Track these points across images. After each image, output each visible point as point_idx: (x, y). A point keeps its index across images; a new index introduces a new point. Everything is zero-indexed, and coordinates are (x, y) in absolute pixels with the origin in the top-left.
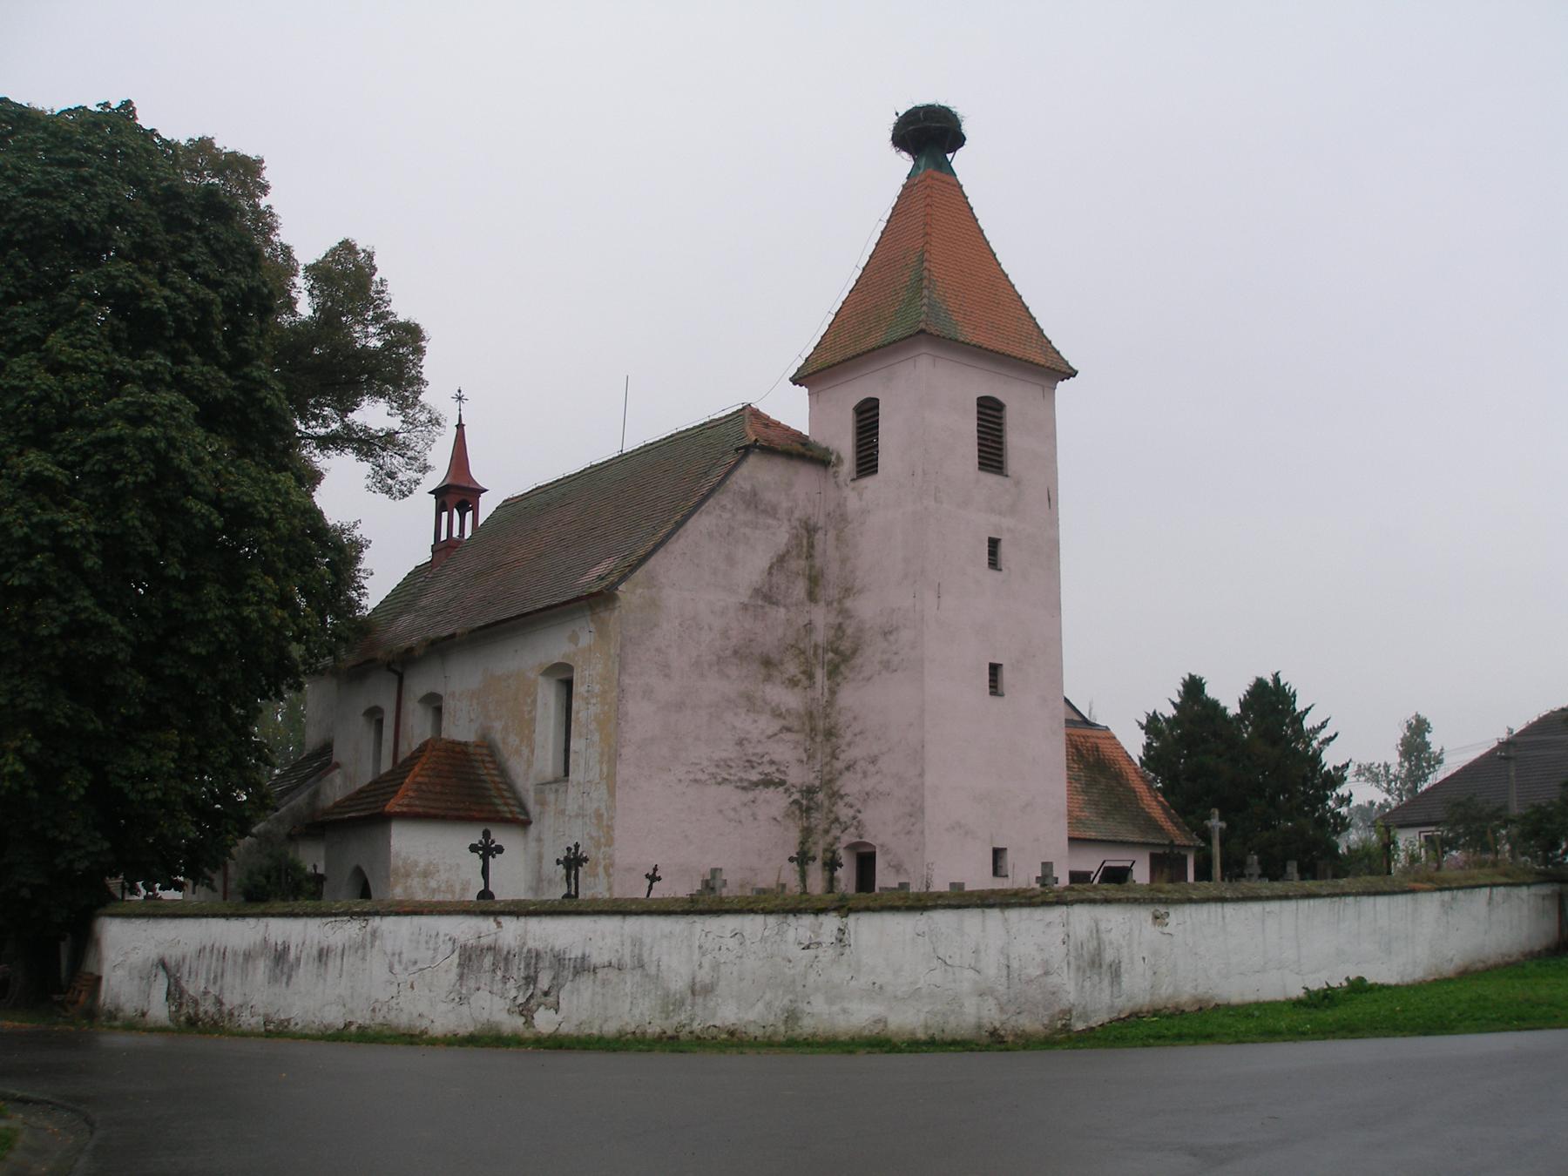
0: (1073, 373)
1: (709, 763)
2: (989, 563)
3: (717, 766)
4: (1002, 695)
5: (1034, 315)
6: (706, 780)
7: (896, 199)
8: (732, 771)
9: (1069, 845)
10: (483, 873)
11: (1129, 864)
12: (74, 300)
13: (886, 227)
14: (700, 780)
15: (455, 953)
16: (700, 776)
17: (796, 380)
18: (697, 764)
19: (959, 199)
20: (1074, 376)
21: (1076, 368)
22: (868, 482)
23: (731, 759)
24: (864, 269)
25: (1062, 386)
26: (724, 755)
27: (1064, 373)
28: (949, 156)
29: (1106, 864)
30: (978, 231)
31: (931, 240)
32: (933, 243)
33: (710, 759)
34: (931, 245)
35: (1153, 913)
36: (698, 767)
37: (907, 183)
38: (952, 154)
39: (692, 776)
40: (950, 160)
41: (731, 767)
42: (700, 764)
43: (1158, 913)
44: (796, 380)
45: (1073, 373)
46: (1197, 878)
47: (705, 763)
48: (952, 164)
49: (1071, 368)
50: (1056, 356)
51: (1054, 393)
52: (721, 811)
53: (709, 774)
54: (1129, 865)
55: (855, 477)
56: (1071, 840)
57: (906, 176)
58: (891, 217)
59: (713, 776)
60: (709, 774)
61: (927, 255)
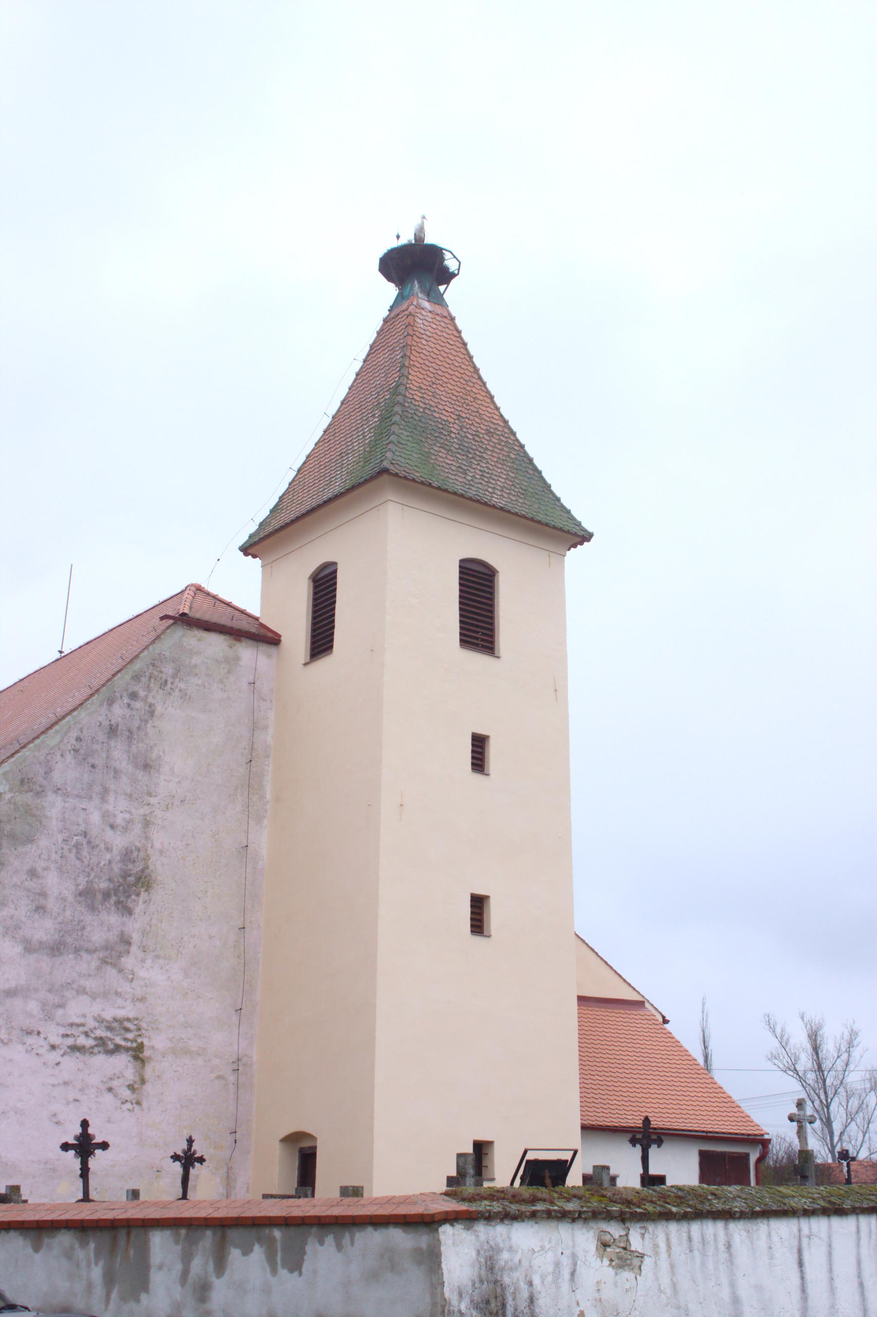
0: (585, 537)
1: (97, 1024)
2: (473, 764)
3: (109, 1028)
4: (489, 936)
5: (540, 468)
6: (92, 1047)
7: (375, 335)
8: (130, 1036)
9: (582, 1133)
10: (81, 1176)
11: (567, 1156)
12: (866, 1081)
13: (362, 368)
14: (84, 1047)
15: (608, 1229)
16: (82, 1041)
17: (246, 550)
18: (78, 1025)
19: (451, 332)
20: (588, 540)
21: (590, 530)
22: (324, 663)
23: (128, 1020)
24: (334, 417)
25: (574, 555)
26: (121, 1013)
27: (576, 535)
28: (442, 288)
29: (530, 1156)
30: (472, 370)
31: (409, 373)
32: (410, 377)
33: (100, 1020)
34: (408, 378)
35: (599, 1239)
36: (81, 1029)
37: (388, 316)
38: (445, 286)
39: (70, 1041)
40: (442, 292)
41: (127, 1030)
42: (83, 1025)
43: (607, 1238)
44: (246, 550)
45: (585, 537)
46: (757, 1183)
47: (91, 1023)
48: (445, 296)
49: (585, 531)
50: (565, 515)
51: (564, 559)
52: (110, 1089)
53: (96, 1039)
54: (569, 1158)
55: (308, 660)
56: (584, 1128)
57: (389, 308)
58: (368, 355)
59: (101, 1042)
60: (96, 1039)
61: (402, 388)
